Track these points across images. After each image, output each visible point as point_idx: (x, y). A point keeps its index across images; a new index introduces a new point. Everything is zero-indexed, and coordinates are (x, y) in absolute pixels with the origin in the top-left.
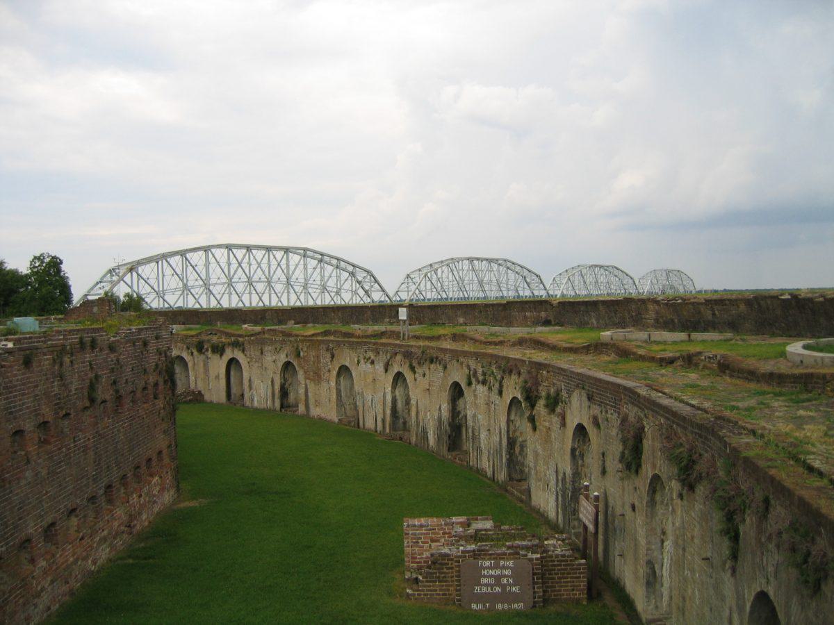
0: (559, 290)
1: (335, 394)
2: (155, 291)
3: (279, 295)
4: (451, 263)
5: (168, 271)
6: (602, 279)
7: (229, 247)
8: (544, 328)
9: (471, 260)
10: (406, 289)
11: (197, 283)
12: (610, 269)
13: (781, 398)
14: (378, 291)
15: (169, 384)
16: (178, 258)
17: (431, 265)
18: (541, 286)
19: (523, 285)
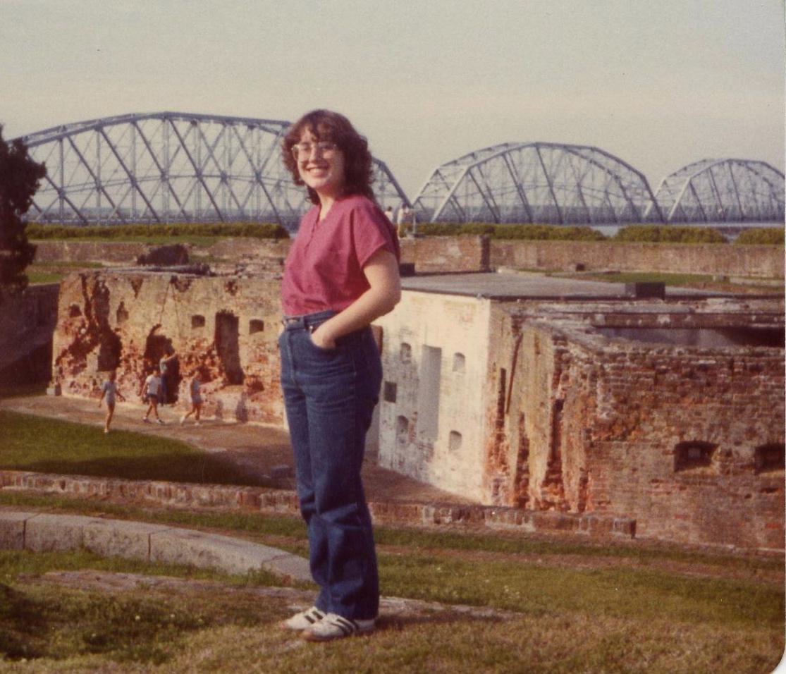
0: (673, 199)
1: (50, 516)
2: (55, 187)
3: (182, 200)
4: (505, 151)
5: (71, 156)
6: (744, 185)
7: (167, 117)
8: (51, 283)
9: (537, 146)
10: (434, 195)
11: (116, 176)
12: (757, 167)
13: (97, 514)
14: (393, 195)
15: (608, 488)
16: (91, 134)
17: (473, 155)
18: (647, 194)
19: (614, 189)
